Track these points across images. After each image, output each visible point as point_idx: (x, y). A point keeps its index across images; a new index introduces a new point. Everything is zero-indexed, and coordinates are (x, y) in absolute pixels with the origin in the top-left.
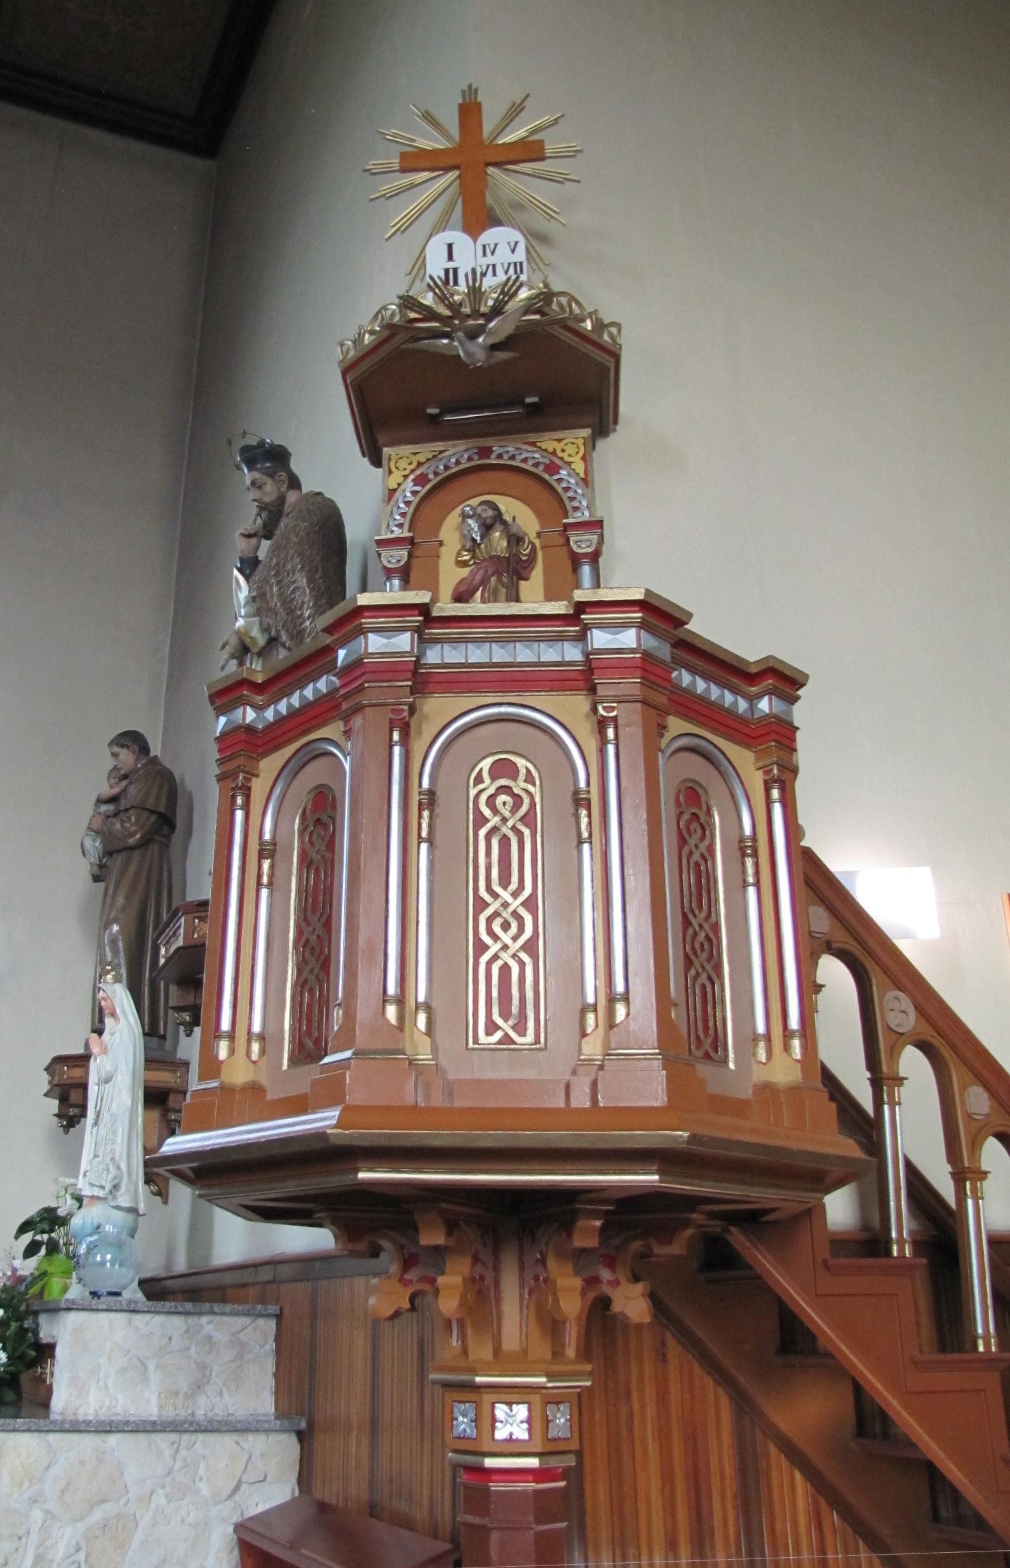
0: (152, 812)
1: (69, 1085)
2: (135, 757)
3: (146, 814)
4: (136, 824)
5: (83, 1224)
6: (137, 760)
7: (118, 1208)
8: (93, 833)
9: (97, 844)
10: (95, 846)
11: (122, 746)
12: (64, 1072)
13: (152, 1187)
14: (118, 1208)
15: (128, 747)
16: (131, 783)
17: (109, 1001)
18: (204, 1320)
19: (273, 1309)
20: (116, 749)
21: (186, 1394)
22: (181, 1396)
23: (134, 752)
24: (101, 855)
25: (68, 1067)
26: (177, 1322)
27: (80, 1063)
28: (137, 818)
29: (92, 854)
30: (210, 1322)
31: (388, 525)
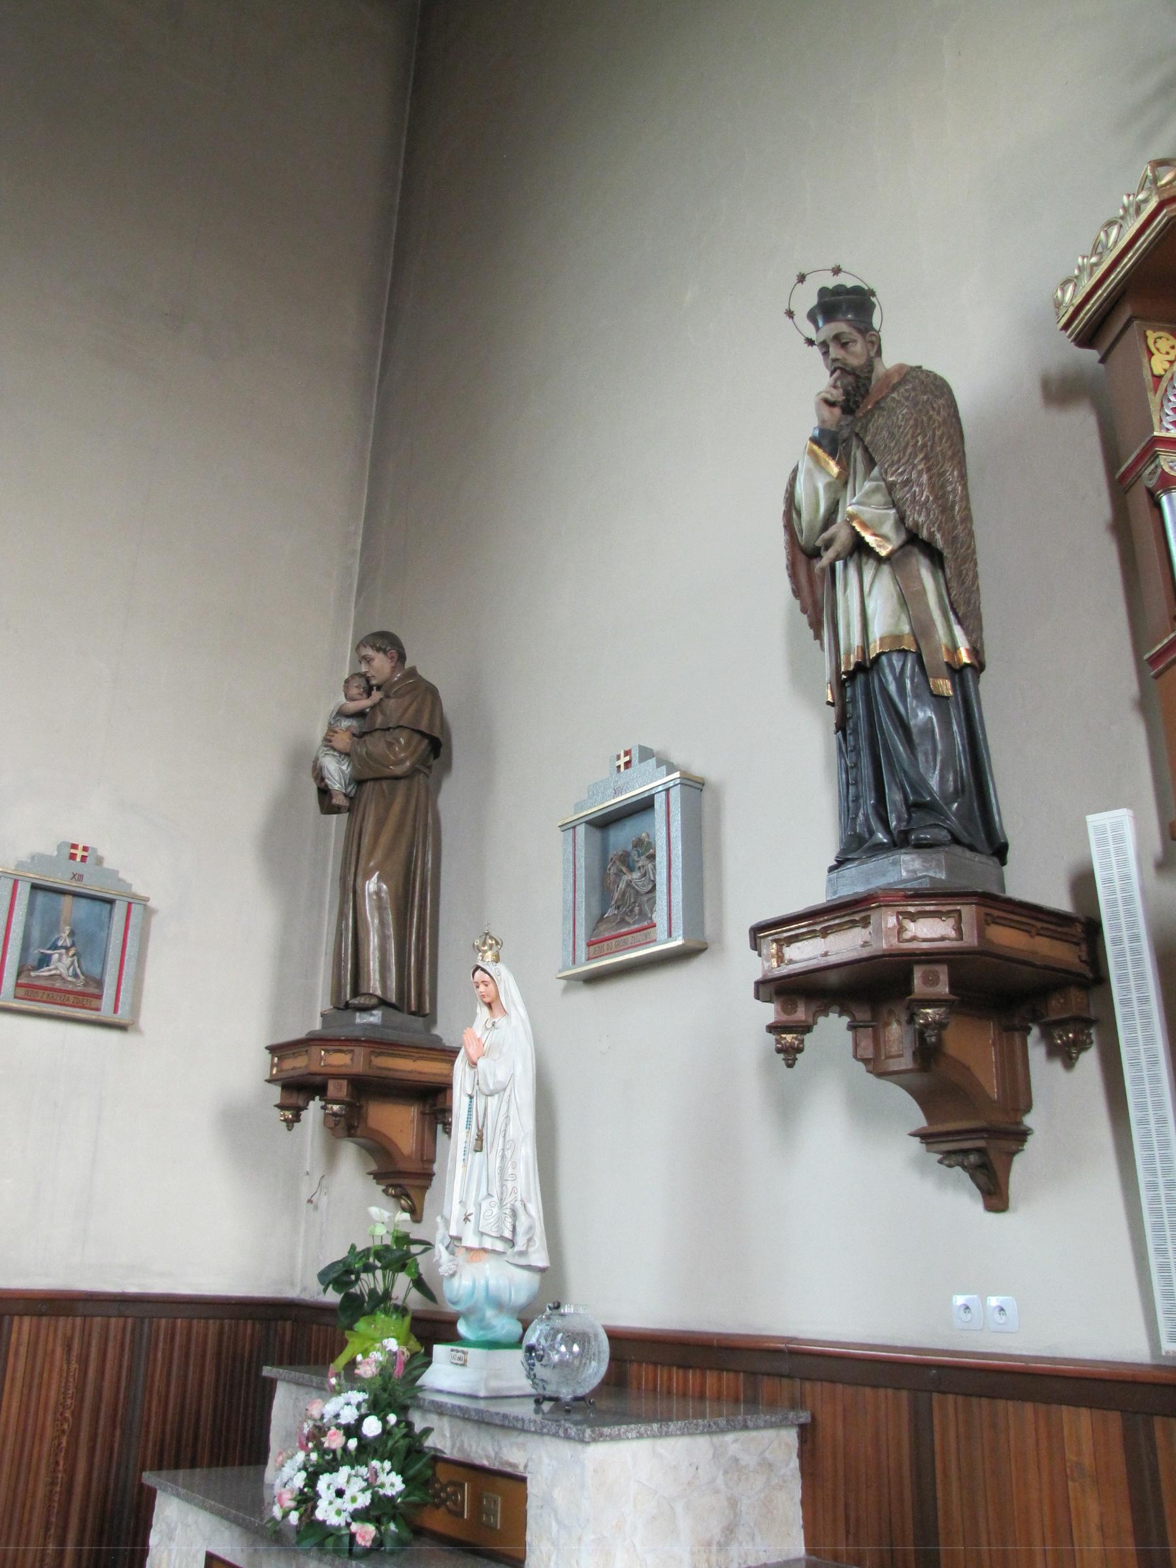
0: (423, 735)
1: (328, 1074)
2: (393, 664)
3: (417, 737)
4: (403, 749)
5: (474, 1285)
6: (394, 669)
7: (529, 1268)
8: (336, 754)
9: (344, 768)
10: (340, 769)
11: (379, 650)
12: (321, 1058)
13: (403, 1202)
14: (529, 1268)
15: (385, 652)
16: (387, 696)
17: (491, 986)
18: (729, 1437)
19: (805, 1417)
20: (369, 652)
21: (719, 1543)
22: (714, 1548)
23: (392, 658)
24: (347, 781)
25: (326, 1051)
26: (702, 1444)
27: (345, 1048)
28: (408, 743)
29: (337, 778)
30: (736, 1441)
31: (1166, 391)
